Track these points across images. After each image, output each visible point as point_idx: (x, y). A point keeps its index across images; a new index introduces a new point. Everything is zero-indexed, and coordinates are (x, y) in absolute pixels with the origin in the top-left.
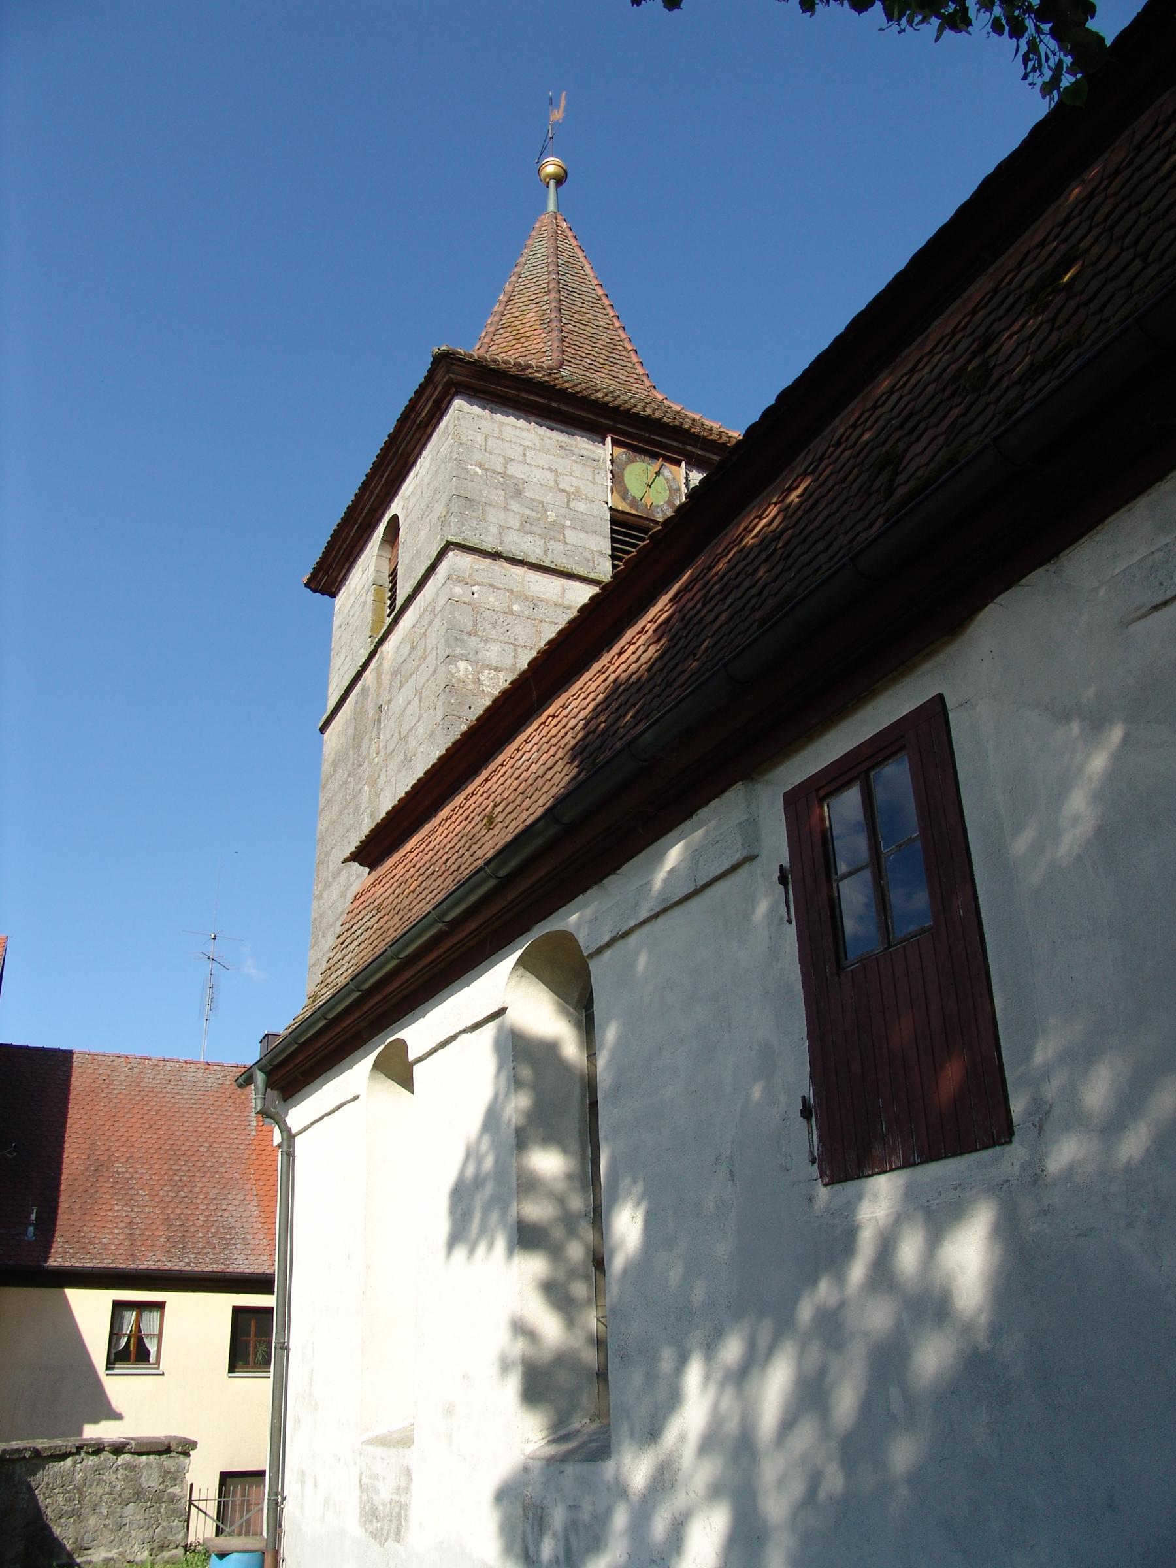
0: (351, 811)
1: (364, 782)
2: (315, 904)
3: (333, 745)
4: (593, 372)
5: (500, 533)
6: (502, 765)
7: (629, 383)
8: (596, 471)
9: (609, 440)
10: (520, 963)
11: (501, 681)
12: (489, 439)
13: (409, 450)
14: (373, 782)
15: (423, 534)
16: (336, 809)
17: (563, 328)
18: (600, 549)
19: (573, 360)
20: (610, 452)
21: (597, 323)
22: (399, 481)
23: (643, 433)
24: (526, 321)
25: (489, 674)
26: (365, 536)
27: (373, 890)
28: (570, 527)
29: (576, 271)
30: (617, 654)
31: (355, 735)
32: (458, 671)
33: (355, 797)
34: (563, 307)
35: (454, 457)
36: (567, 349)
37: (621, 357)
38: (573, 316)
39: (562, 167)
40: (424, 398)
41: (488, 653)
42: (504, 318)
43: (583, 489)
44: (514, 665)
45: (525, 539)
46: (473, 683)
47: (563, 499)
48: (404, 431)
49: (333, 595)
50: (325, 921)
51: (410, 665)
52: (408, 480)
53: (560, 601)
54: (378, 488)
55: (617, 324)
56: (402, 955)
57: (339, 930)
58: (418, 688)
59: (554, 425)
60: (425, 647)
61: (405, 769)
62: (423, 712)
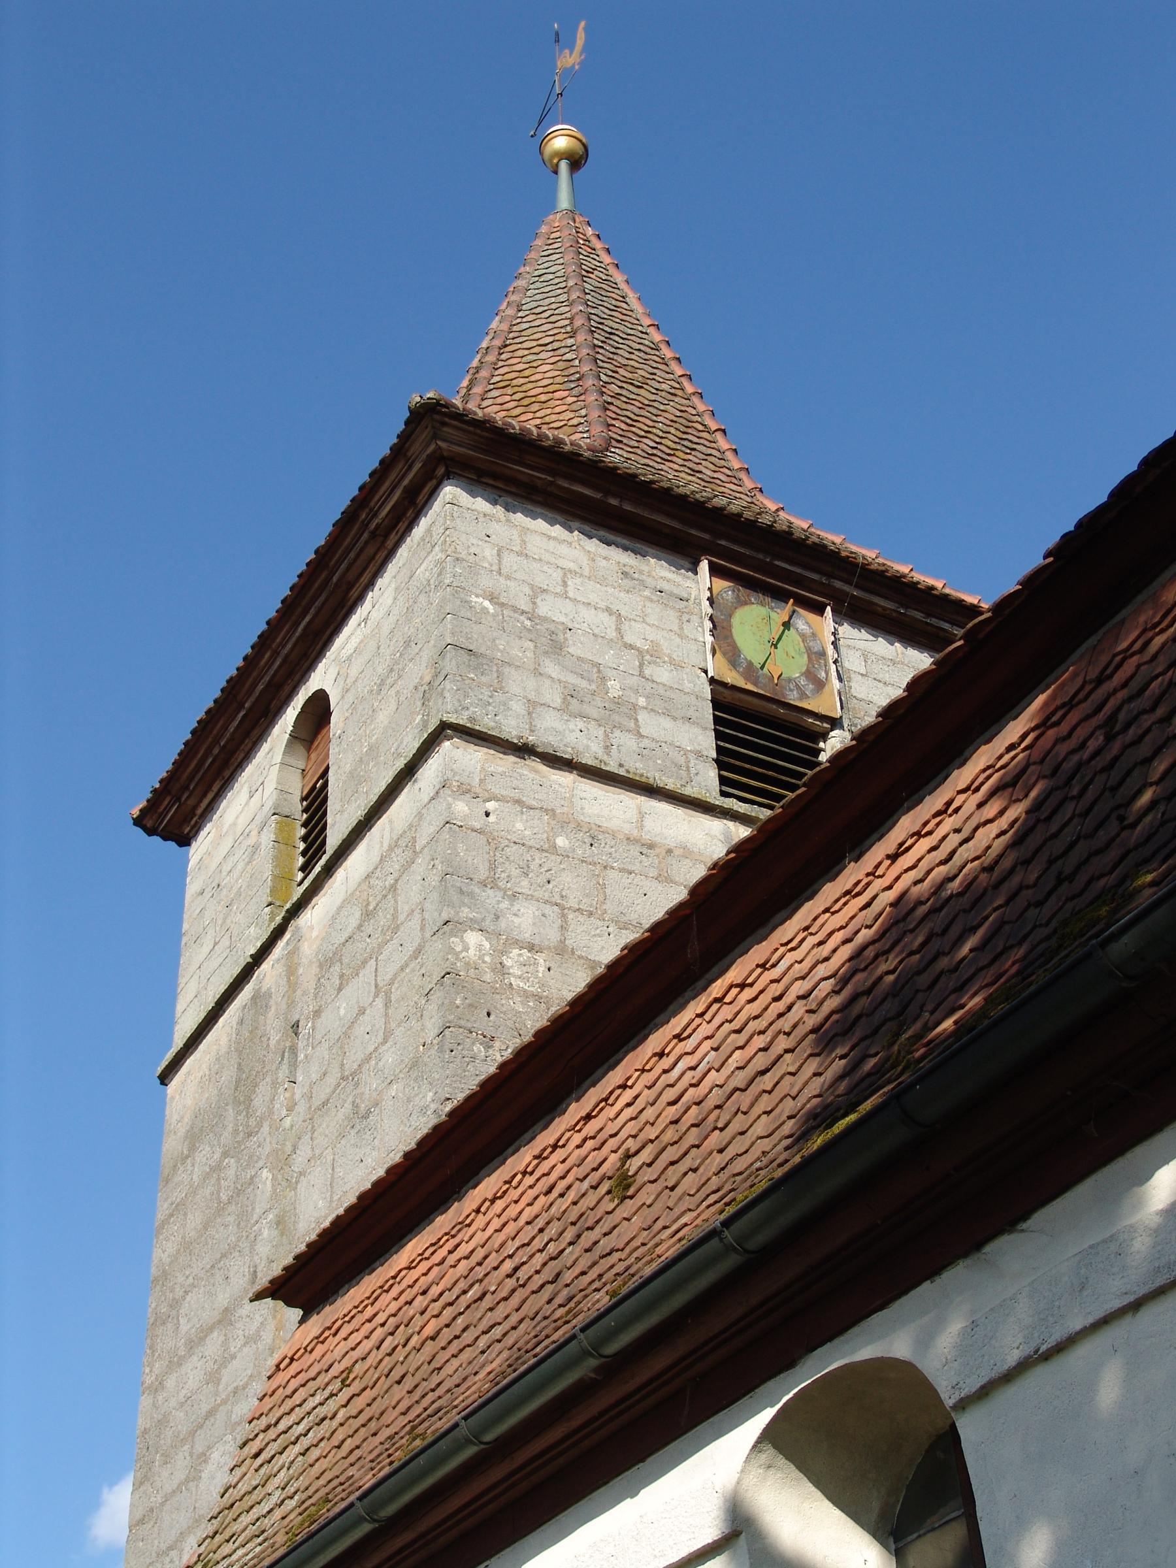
0: (231, 1219)
1: (261, 1164)
2: (146, 1401)
3: (189, 1102)
4: (659, 460)
5: (529, 713)
6: (624, 1086)
7: (718, 482)
8: (685, 617)
9: (704, 566)
10: (769, 1436)
11: (541, 969)
12: (505, 554)
13: (351, 576)
14: (281, 1162)
15: (383, 718)
16: (194, 1219)
17: (604, 389)
18: (698, 748)
19: (625, 441)
20: (708, 585)
21: (657, 385)
22: (328, 633)
23: (761, 556)
24: (538, 377)
25: (520, 955)
26: (256, 732)
27: (320, 1349)
28: (644, 708)
29: (614, 302)
30: (888, 857)
31: (238, 1081)
32: (466, 949)
33: (239, 1192)
34: (600, 357)
35: (447, 581)
36: (614, 422)
37: (702, 441)
38: (616, 372)
39: (580, 141)
40: (387, 484)
41: (517, 920)
42: (497, 373)
43: (665, 647)
44: (562, 942)
45: (571, 725)
46: (493, 970)
47: (630, 661)
48: (346, 543)
49: (185, 841)
50: (169, 1433)
51: (361, 945)
52: (346, 631)
53: (635, 833)
54: (289, 646)
55: (690, 389)
56: (489, 1437)
57: (246, 1430)
58: (381, 984)
59: (611, 537)
60: (396, 909)
61: (353, 1132)
62: (393, 1025)
